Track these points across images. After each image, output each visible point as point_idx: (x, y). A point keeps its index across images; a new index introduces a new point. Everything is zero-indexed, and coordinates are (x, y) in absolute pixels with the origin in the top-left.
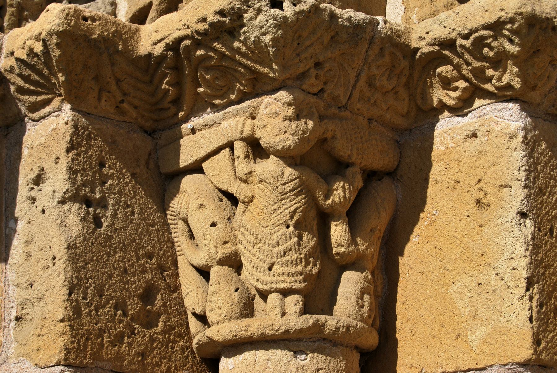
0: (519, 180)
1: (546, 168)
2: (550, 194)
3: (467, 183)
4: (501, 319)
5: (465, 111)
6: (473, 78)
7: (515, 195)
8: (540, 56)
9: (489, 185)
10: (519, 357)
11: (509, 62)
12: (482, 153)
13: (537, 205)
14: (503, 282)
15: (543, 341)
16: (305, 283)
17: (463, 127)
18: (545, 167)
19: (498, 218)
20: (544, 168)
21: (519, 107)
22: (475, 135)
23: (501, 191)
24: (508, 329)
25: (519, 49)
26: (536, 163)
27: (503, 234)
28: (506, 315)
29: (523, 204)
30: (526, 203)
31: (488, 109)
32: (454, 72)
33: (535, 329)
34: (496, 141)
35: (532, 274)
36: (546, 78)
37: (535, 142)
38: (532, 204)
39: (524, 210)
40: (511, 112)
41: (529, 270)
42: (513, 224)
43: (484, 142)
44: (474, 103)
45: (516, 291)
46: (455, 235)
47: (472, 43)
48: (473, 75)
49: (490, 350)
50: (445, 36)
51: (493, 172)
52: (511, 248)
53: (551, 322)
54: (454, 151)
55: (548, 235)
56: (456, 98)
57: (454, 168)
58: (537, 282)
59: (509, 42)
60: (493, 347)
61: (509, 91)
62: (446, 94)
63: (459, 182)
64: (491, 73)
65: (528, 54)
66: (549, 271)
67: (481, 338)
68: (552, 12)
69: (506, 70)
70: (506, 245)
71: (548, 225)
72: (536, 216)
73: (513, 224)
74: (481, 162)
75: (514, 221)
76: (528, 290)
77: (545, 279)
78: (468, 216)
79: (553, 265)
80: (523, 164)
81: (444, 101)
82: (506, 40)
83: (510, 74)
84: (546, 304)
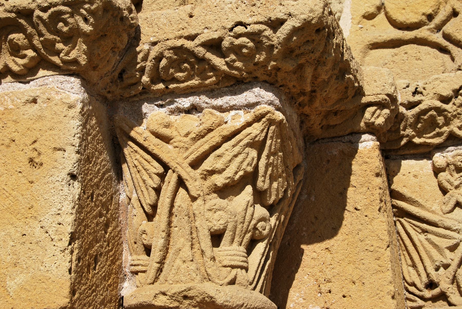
0: (74, 146)
1: (94, 141)
2: (94, 164)
3: (22, 142)
4: (42, 268)
5: (27, 79)
6: (42, 49)
7: (68, 158)
8: (106, 41)
9: (43, 146)
10: (55, 304)
11: (79, 39)
12: (40, 118)
13: (85, 170)
14: (47, 234)
15: (77, 292)
16: (176, 55)
17: (25, 92)
18: (93, 139)
19: (49, 177)
20: (92, 140)
21: (80, 82)
22: (35, 101)
23: (54, 153)
24: (48, 278)
25: (92, 29)
26: (88, 134)
27: (52, 191)
28: (47, 265)
29: (75, 167)
30: (77, 166)
31: (51, 79)
32: (25, 41)
33: (73, 280)
34: (55, 108)
35: (76, 230)
36: (106, 62)
37: (88, 116)
38: (81, 168)
39: (75, 173)
40: (72, 85)
41: (73, 226)
42: (63, 183)
43: (44, 108)
44: (38, 73)
45: (59, 244)
46: (5, 188)
47: (49, 16)
48: (42, 46)
49: (28, 296)
50: (24, 5)
51: (49, 136)
52: (59, 205)
53: (85, 276)
54: (13, 113)
55: (90, 199)
56: (22, 65)
57: (12, 127)
58: (78, 239)
59: (84, 21)
60: (31, 293)
61: (74, 66)
62: (13, 60)
63: (14, 141)
64: (60, 46)
65: (97, 36)
66: (88, 231)
67: (20, 284)
68: (122, 5)
69: (76, 46)
70: (54, 201)
71: (90, 190)
72: (83, 179)
73: (63, 183)
74: (38, 125)
75: (64, 181)
76: (70, 244)
77: (84, 237)
78: (20, 172)
79: (90, 226)
80: (78, 132)
81: (10, 66)
82: (81, 19)
83: (78, 50)
84: (83, 260)
